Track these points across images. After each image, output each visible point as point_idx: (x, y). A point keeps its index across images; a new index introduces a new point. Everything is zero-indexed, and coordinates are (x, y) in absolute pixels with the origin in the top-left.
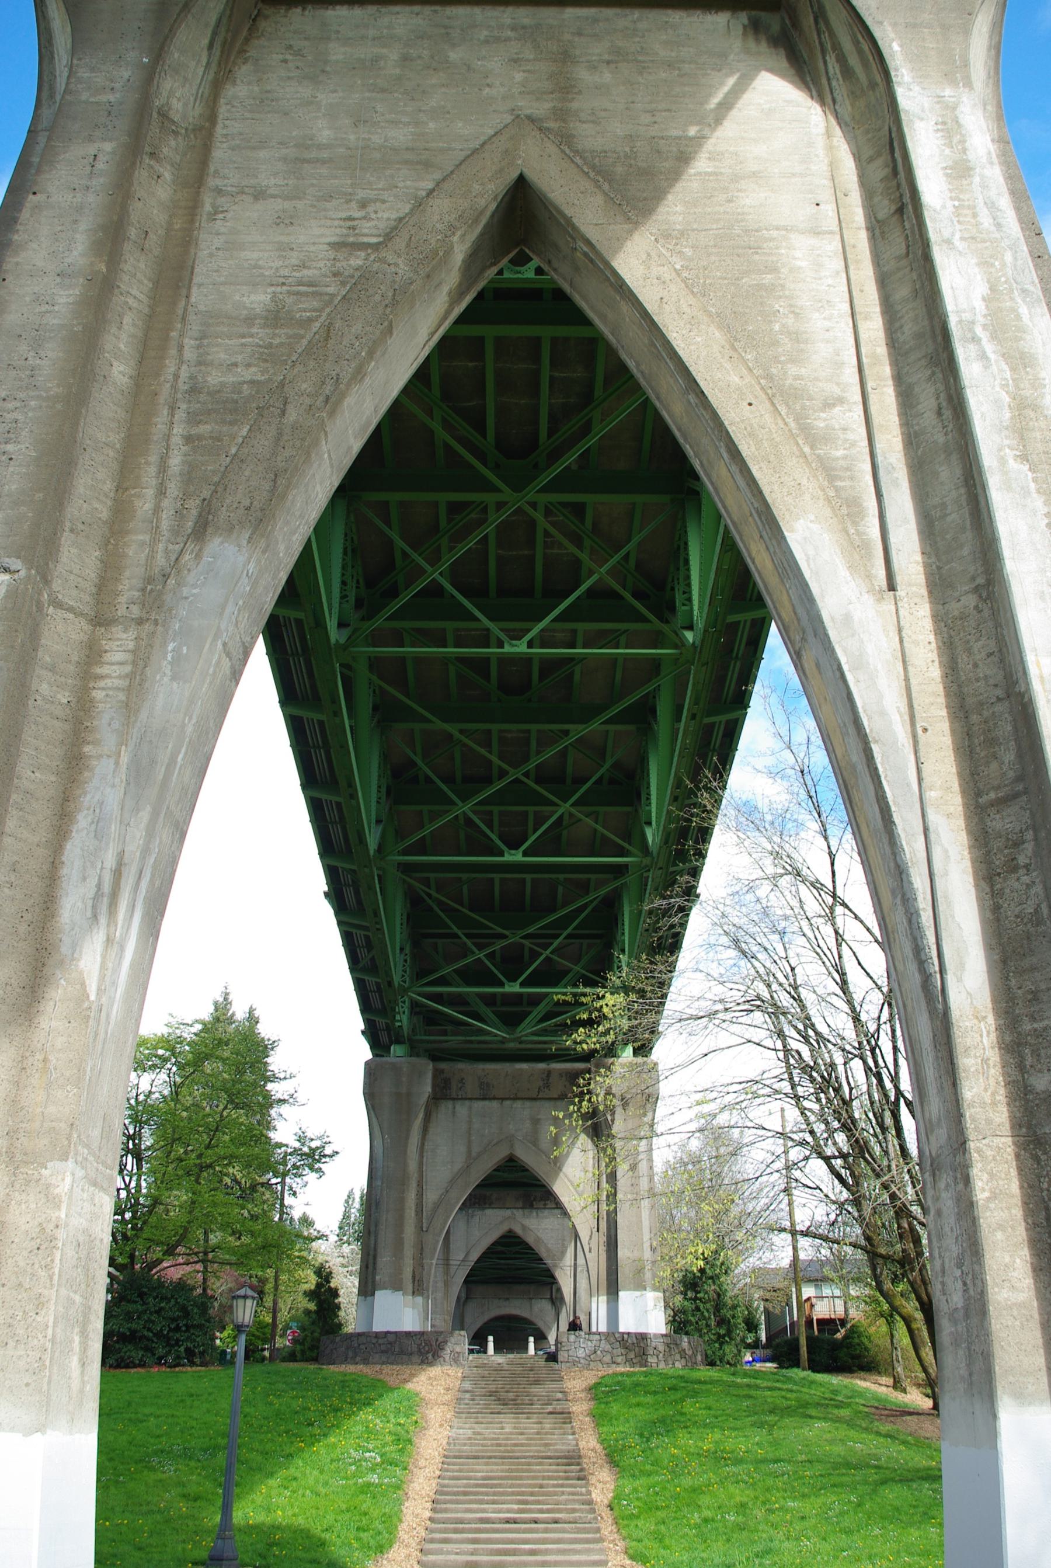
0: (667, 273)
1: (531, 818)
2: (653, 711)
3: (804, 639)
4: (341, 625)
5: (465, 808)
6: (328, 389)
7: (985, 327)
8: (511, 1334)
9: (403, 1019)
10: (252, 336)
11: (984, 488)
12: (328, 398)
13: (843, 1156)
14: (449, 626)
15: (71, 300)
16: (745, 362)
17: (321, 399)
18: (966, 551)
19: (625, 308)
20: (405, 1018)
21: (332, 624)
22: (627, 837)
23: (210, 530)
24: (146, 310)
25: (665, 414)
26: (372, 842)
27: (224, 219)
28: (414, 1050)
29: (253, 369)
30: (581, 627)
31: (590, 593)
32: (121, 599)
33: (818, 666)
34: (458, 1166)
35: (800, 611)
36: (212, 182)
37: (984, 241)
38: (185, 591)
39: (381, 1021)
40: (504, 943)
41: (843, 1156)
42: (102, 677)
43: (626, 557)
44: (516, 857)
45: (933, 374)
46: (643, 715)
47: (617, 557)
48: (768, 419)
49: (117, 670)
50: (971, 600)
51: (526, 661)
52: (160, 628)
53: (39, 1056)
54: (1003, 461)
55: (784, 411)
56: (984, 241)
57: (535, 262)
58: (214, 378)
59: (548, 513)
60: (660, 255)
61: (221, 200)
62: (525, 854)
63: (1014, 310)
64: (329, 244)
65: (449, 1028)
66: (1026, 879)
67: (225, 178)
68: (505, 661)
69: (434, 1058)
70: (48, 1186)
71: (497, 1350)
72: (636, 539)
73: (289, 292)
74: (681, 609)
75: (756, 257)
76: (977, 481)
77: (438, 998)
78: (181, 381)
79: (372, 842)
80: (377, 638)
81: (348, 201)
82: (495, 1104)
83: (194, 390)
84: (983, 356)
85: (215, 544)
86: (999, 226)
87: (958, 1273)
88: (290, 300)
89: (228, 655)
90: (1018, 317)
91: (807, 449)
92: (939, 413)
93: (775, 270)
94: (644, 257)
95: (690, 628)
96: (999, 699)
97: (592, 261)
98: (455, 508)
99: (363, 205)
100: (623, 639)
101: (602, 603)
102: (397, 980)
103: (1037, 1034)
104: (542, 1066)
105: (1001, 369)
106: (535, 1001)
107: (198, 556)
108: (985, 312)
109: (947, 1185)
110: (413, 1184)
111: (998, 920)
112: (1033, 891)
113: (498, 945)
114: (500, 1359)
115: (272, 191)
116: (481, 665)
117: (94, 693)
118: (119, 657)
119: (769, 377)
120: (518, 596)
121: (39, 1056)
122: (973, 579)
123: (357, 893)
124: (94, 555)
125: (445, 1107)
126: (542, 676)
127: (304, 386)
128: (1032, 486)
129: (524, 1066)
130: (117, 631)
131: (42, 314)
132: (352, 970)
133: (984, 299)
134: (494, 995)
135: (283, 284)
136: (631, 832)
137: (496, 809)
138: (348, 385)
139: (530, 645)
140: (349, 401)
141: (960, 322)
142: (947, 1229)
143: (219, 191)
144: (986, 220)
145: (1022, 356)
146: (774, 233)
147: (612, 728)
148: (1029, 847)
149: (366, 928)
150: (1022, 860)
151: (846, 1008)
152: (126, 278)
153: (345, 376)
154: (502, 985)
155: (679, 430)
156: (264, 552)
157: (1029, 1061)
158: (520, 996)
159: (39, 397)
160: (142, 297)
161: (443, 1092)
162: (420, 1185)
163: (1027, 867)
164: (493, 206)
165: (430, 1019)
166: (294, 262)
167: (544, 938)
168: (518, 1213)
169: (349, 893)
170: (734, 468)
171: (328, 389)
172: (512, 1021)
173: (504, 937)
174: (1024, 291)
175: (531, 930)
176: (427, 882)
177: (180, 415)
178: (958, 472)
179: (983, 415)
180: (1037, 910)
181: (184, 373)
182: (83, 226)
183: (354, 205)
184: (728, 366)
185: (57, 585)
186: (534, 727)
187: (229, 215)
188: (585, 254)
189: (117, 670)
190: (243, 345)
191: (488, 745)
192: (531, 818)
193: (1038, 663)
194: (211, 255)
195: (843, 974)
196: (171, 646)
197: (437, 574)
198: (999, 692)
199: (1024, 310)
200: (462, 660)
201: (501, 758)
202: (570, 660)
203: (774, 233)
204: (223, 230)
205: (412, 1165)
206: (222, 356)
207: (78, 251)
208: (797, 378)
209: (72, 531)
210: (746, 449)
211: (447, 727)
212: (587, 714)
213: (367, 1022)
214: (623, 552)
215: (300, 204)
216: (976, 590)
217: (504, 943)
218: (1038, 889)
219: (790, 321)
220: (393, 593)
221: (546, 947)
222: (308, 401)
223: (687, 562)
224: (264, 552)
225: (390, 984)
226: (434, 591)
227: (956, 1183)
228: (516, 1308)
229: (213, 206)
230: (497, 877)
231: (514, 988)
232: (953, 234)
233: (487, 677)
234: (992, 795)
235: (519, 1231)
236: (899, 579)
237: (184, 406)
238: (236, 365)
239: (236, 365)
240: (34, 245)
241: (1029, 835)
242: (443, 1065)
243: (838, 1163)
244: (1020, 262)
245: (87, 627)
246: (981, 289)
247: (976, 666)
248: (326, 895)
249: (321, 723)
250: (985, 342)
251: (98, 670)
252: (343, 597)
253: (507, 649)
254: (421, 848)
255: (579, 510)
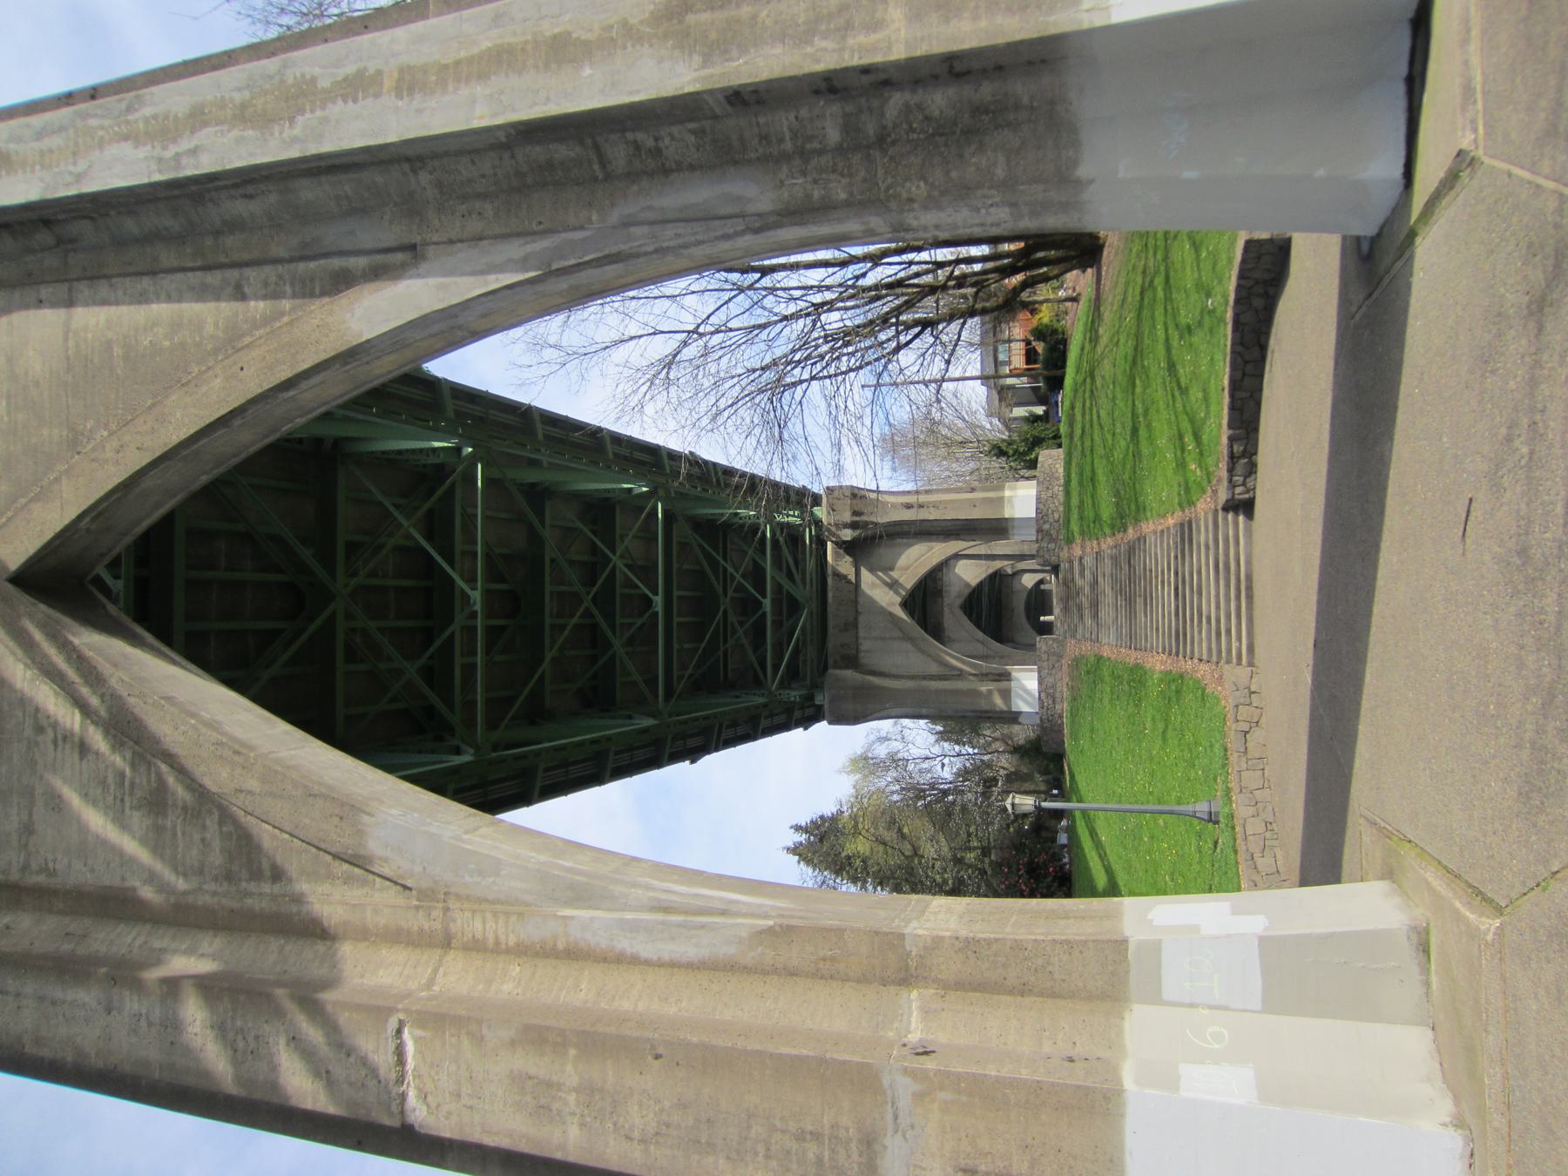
0: (113, 444)
1: (627, 591)
2: (533, 485)
3: (460, 327)
4: (458, 751)
5: (617, 644)
6: (227, 753)
7: (165, 148)
8: (1039, 601)
9: (794, 695)
10: (174, 827)
11: (320, 157)
12: (237, 753)
13: (898, 333)
14: (458, 660)
15: (135, 998)
16: (201, 373)
17: (236, 758)
18: (379, 179)
19: (147, 483)
20: (793, 693)
21: (458, 760)
22: (641, 509)
23: (362, 852)
24: (148, 927)
25: (253, 450)
26: (648, 722)
27: (54, 861)
28: (817, 686)
29: (208, 822)
30: (459, 546)
31: (429, 538)
32: (426, 927)
33: (484, 316)
34: (909, 646)
35: (436, 328)
36: (15, 876)
37: (76, 144)
38: (418, 869)
39: (797, 714)
40: (730, 611)
41: (898, 333)
42: (497, 938)
43: (396, 506)
44: (658, 600)
45: (211, 200)
46: (538, 495)
47: (396, 514)
48: (255, 353)
49: (491, 925)
50: (424, 177)
51: (487, 593)
52: (452, 890)
53: (821, 965)
54: (295, 140)
55: (247, 340)
56: (76, 144)
57: (101, 571)
58: (216, 859)
59: (354, 574)
60: (94, 450)
61: (34, 866)
62: (656, 594)
63: (146, 121)
64: (81, 760)
65: (801, 658)
66: (667, 141)
67: (10, 863)
68: (490, 612)
69: (826, 669)
70: (925, 948)
71: (1051, 613)
72: (380, 497)
73: (131, 794)
74: (442, 458)
75: (96, 360)
76: (313, 164)
77: (776, 668)
78: (220, 890)
79: (648, 722)
80: (470, 723)
81: (37, 744)
82: (861, 619)
83: (229, 877)
84: (194, 152)
85: (374, 846)
86: (62, 129)
87: (983, 211)
88: (139, 793)
89: (476, 829)
90: (155, 117)
91: (286, 319)
92: (250, 197)
93: (109, 345)
94: (95, 465)
95: (458, 450)
96: (513, 157)
97: (100, 514)
98: (351, 656)
99: (40, 730)
100: (469, 511)
101: (438, 526)
102: (761, 700)
103: (795, 136)
104: (830, 580)
105: (204, 136)
106: (778, 588)
107: (386, 860)
108: (149, 147)
109: (916, 218)
110: (925, 683)
111: (701, 167)
112: (676, 134)
113: (733, 618)
114: (1057, 610)
115: (25, 818)
116: (493, 633)
117: (511, 943)
118: (478, 925)
119: (216, 351)
120: (432, 598)
121: (821, 965)
122: (405, 174)
123: (692, 736)
124: (387, 953)
125: (865, 659)
126: (502, 580)
127: (224, 775)
128: (318, 113)
129: (830, 595)
130: (453, 928)
131: (150, 1024)
132: (755, 738)
133: (136, 147)
134: (773, 622)
135: (122, 800)
136: (635, 504)
137: (619, 620)
138: (224, 734)
139: (474, 589)
140: (239, 733)
141: (160, 172)
142: (949, 220)
143: (25, 868)
144: (56, 141)
145: (192, 115)
146: (71, 343)
147: (548, 521)
148: (640, 136)
149: (721, 725)
150: (650, 143)
151: (779, 326)
152: (115, 949)
153: (215, 736)
154: (764, 614)
155: (267, 436)
156: (382, 802)
157: (816, 145)
158: (773, 600)
159: (232, 1018)
160: (134, 933)
161: (852, 661)
162: (924, 678)
163: (656, 139)
164: (43, 607)
165: (793, 674)
166: (99, 791)
167: (726, 579)
168: (947, 601)
169: (692, 743)
170: (304, 385)
171: (227, 753)
172: (794, 607)
173: (725, 612)
174: (129, 109)
175: (720, 590)
176: (680, 678)
177: (252, 887)
178: (305, 182)
179: (251, 155)
180: (693, 132)
181: (212, 887)
182: (58, 993)
183: (40, 738)
184: (204, 389)
185: (413, 985)
186: (548, 588)
187: (50, 857)
188: (93, 520)
189: (491, 925)
190: (184, 833)
191: (563, 627)
192: (627, 591)
193: (481, 118)
194: (92, 870)
195: (754, 327)
196: (468, 879)
197: (411, 670)
198: (506, 155)
199: (148, 111)
200: (489, 650)
201: (572, 616)
202: (488, 557)
203: (71, 343)
204: (66, 861)
205: (909, 684)
206: (195, 852)
207: (86, 996)
208: (216, 324)
209: (362, 976)
210: (285, 373)
211: (547, 660)
212: (535, 539)
213: (797, 726)
214: (391, 508)
215: (39, 791)
216: (414, 171)
217: (730, 611)
218: (675, 130)
219: (160, 331)
220: (430, 711)
221: (733, 578)
222: (238, 771)
223: (400, 452)
224: (382, 802)
225: (765, 705)
226: (428, 673)
227: (913, 210)
228: (1019, 604)
229: (39, 872)
230: (676, 620)
231: (767, 603)
232: (70, 173)
233: (503, 628)
234: (596, 167)
235: (959, 602)
236: (406, 241)
237: (244, 884)
238: (203, 840)
239: (203, 840)
240: (79, 1039)
241: (630, 136)
242: (831, 662)
243: (903, 339)
244: (99, 112)
245: (452, 954)
246: (127, 149)
247: (483, 176)
248: (693, 762)
249: (547, 770)
250: (179, 150)
251: (491, 941)
252: (433, 752)
253: (478, 607)
254: (652, 682)
255: (352, 547)
